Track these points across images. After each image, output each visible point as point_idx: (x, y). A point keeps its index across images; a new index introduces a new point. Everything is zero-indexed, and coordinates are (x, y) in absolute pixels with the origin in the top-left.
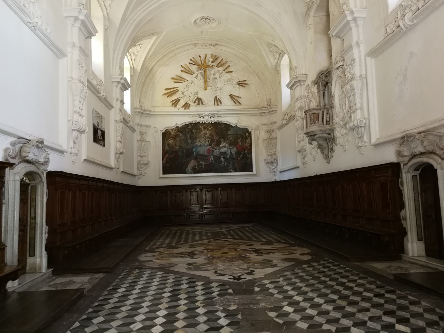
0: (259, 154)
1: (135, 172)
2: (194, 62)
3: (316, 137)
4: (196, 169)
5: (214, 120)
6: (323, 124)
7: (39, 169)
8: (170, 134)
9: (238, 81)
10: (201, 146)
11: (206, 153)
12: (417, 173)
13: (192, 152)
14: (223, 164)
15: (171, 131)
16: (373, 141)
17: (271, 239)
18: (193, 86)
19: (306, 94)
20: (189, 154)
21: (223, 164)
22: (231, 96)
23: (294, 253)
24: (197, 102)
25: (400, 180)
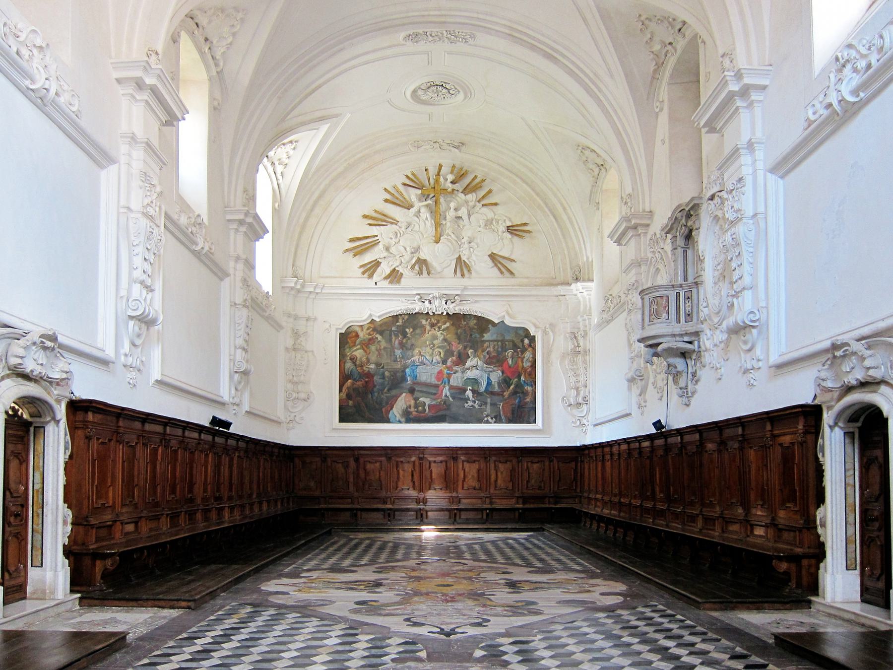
0: (551, 386)
1: (280, 413)
2: (413, 182)
3: (660, 348)
4: (410, 413)
5: (453, 308)
6: (678, 321)
7: (49, 393)
8: (357, 336)
9: (509, 224)
10: (423, 363)
11: (434, 381)
12: (855, 427)
13: (404, 379)
14: (470, 403)
15: (358, 329)
16: (774, 359)
17: (553, 563)
18: (411, 232)
19: (650, 255)
20: (397, 381)
21: (470, 403)
22: (493, 256)
23: (589, 591)
24: (417, 267)
25: (820, 441)
